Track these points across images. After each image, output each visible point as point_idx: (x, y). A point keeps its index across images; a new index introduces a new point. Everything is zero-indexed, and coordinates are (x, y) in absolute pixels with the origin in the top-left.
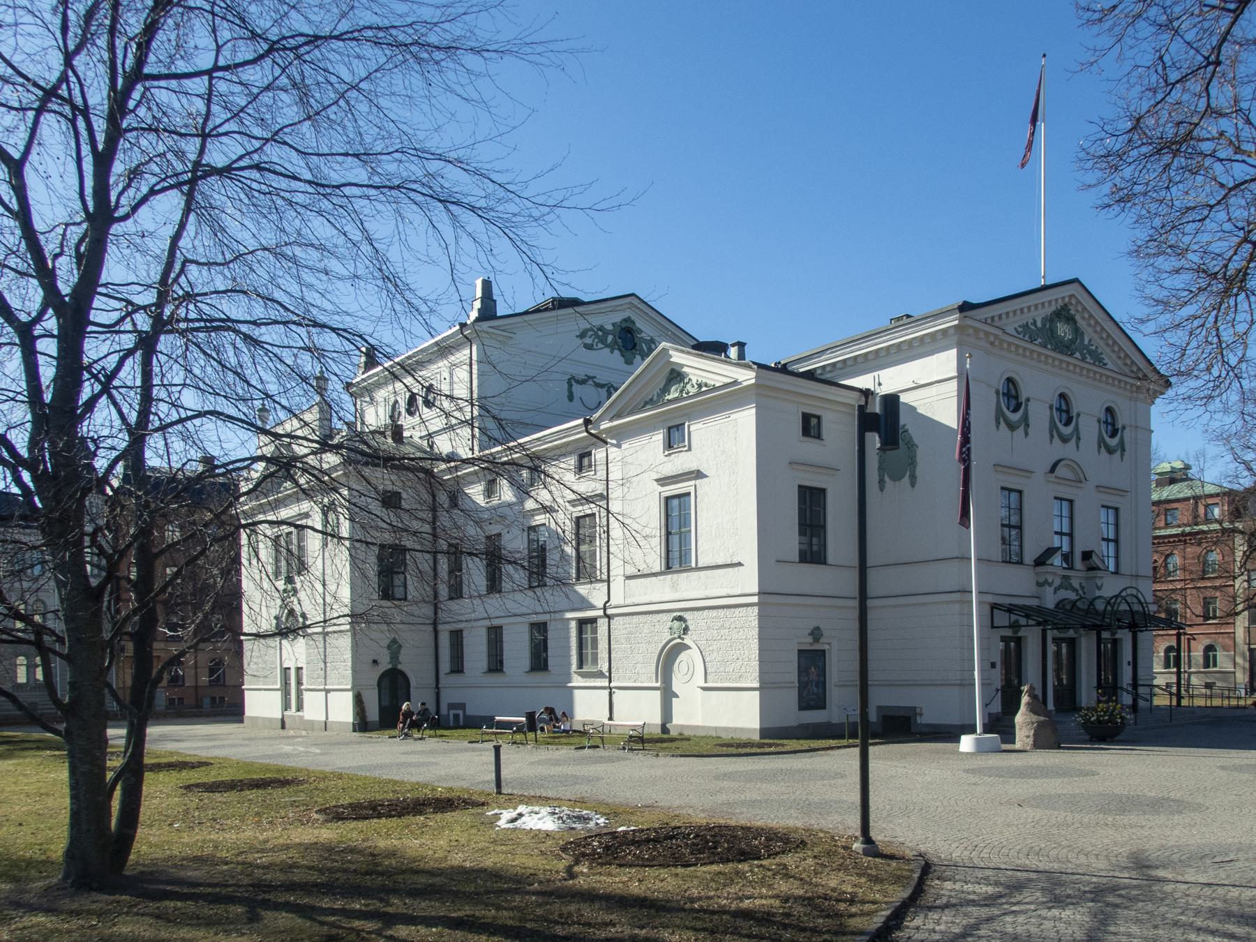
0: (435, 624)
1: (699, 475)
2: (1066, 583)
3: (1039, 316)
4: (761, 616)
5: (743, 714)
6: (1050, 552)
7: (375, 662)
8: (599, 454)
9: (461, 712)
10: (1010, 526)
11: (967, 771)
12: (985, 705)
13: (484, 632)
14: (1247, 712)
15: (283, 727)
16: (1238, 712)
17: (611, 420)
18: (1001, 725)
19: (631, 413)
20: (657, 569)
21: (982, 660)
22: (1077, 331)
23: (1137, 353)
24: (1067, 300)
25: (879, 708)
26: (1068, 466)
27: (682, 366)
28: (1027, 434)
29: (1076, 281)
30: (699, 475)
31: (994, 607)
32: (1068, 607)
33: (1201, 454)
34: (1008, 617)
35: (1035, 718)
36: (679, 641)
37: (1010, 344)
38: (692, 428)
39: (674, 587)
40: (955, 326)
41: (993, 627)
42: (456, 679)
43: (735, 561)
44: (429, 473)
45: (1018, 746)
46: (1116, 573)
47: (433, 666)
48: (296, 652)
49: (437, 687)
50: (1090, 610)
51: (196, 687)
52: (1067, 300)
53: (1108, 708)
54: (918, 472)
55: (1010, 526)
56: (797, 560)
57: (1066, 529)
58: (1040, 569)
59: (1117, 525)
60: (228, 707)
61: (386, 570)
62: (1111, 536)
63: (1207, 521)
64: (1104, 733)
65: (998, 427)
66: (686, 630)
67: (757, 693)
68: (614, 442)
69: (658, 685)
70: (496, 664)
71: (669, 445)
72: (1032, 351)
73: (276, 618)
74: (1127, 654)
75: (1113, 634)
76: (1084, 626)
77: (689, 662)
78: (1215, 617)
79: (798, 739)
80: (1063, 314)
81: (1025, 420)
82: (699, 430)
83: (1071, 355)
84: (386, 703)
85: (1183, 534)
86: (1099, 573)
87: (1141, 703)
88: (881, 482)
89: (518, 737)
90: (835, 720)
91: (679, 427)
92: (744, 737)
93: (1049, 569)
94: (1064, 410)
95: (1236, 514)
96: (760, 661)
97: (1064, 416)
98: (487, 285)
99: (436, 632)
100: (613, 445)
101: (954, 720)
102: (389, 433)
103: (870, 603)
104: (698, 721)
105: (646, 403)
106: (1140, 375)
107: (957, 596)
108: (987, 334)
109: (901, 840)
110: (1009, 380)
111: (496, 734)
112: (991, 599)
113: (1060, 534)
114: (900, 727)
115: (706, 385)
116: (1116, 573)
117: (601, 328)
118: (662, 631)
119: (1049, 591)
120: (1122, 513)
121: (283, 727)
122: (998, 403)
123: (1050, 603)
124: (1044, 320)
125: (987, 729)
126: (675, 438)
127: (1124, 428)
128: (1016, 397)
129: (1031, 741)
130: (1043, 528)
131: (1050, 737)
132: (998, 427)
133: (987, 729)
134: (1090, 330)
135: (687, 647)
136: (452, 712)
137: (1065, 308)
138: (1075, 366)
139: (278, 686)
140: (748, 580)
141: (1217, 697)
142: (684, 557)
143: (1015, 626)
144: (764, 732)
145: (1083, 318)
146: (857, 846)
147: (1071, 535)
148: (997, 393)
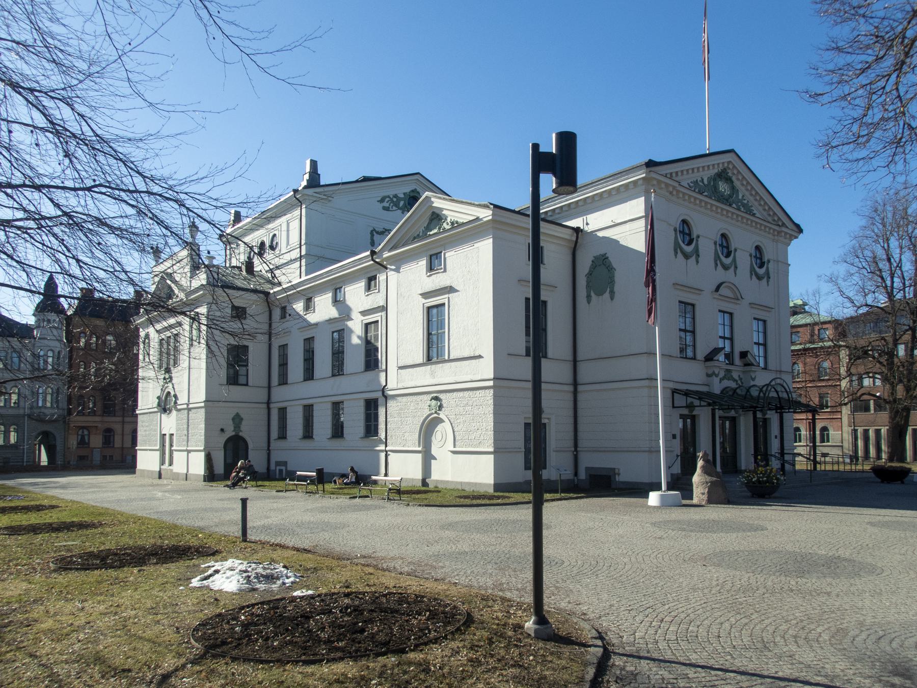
0: (268, 403)
1: (450, 290)
2: (728, 375)
3: (706, 175)
4: (495, 397)
5: (481, 472)
6: (717, 351)
7: (222, 430)
8: (382, 277)
9: (283, 468)
10: (685, 331)
11: (654, 524)
12: (669, 467)
13: (301, 409)
14: (864, 475)
15: (160, 477)
16: (858, 475)
17: (390, 251)
18: (680, 484)
19: (404, 246)
20: (420, 361)
21: (665, 432)
22: (733, 188)
23: (777, 207)
24: (726, 165)
25: (587, 469)
26: (729, 288)
27: (442, 209)
28: (697, 262)
29: (732, 151)
30: (450, 290)
31: (674, 391)
32: (731, 393)
33: (817, 293)
34: (685, 399)
35: (708, 478)
36: (435, 415)
37: (684, 194)
38: (447, 255)
39: (433, 374)
40: (643, 178)
41: (673, 407)
42: (282, 444)
43: (477, 354)
44: (267, 294)
45: (695, 501)
46: (765, 368)
47: (266, 434)
48: (170, 423)
49: (269, 449)
50: (747, 396)
51: (123, 448)
52: (726, 165)
53: (766, 471)
54: (616, 289)
55: (685, 331)
56: (524, 353)
57: (727, 335)
58: (709, 364)
59: (765, 333)
60: (122, 460)
61: (233, 365)
62: (761, 341)
63: (822, 340)
64: (762, 492)
65: (676, 256)
66: (440, 407)
67: (492, 456)
68: (393, 267)
69: (420, 449)
70: (308, 434)
71: (431, 268)
72: (701, 201)
73: (159, 398)
74: (774, 430)
75: (764, 414)
76: (743, 408)
77: (443, 432)
78: (827, 407)
79: (523, 492)
80: (723, 175)
81: (696, 252)
82: (453, 257)
83: (730, 205)
84: (230, 461)
85: (805, 349)
86: (753, 368)
87: (787, 466)
88: (589, 297)
89: (312, 488)
90: (553, 478)
91: (437, 255)
92: (482, 490)
93: (716, 363)
94: (725, 245)
95: (843, 335)
96: (495, 431)
97: (725, 250)
98: (314, 164)
99: (269, 409)
100: (391, 270)
101: (646, 479)
102: (244, 268)
103: (580, 388)
104: (448, 478)
105: (415, 238)
106: (780, 223)
107: (646, 383)
108: (667, 185)
109: (584, 608)
110: (684, 222)
111: (296, 485)
112: (672, 385)
113: (724, 338)
114: (600, 484)
115: (457, 222)
116: (765, 368)
117: (395, 196)
118: (422, 408)
119: (716, 380)
120: (769, 324)
121: (160, 477)
122: (676, 238)
123: (717, 390)
124: (709, 179)
125: (670, 487)
126: (434, 263)
127: (769, 261)
128: (690, 235)
129: (705, 497)
130: (712, 331)
131: (721, 495)
132: (676, 256)
133: (670, 487)
134: (743, 188)
135: (442, 421)
136: (278, 468)
137: (724, 171)
138: (733, 213)
139: (158, 448)
140: (486, 369)
141: (829, 463)
142: (440, 353)
143: (690, 407)
144: (498, 487)
145: (738, 179)
146: (530, 624)
147: (731, 339)
148: (675, 230)
